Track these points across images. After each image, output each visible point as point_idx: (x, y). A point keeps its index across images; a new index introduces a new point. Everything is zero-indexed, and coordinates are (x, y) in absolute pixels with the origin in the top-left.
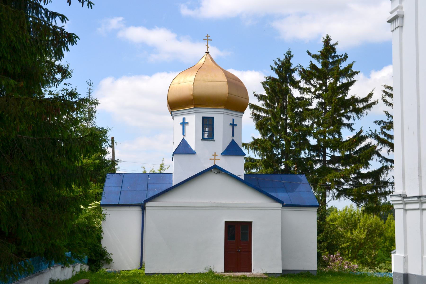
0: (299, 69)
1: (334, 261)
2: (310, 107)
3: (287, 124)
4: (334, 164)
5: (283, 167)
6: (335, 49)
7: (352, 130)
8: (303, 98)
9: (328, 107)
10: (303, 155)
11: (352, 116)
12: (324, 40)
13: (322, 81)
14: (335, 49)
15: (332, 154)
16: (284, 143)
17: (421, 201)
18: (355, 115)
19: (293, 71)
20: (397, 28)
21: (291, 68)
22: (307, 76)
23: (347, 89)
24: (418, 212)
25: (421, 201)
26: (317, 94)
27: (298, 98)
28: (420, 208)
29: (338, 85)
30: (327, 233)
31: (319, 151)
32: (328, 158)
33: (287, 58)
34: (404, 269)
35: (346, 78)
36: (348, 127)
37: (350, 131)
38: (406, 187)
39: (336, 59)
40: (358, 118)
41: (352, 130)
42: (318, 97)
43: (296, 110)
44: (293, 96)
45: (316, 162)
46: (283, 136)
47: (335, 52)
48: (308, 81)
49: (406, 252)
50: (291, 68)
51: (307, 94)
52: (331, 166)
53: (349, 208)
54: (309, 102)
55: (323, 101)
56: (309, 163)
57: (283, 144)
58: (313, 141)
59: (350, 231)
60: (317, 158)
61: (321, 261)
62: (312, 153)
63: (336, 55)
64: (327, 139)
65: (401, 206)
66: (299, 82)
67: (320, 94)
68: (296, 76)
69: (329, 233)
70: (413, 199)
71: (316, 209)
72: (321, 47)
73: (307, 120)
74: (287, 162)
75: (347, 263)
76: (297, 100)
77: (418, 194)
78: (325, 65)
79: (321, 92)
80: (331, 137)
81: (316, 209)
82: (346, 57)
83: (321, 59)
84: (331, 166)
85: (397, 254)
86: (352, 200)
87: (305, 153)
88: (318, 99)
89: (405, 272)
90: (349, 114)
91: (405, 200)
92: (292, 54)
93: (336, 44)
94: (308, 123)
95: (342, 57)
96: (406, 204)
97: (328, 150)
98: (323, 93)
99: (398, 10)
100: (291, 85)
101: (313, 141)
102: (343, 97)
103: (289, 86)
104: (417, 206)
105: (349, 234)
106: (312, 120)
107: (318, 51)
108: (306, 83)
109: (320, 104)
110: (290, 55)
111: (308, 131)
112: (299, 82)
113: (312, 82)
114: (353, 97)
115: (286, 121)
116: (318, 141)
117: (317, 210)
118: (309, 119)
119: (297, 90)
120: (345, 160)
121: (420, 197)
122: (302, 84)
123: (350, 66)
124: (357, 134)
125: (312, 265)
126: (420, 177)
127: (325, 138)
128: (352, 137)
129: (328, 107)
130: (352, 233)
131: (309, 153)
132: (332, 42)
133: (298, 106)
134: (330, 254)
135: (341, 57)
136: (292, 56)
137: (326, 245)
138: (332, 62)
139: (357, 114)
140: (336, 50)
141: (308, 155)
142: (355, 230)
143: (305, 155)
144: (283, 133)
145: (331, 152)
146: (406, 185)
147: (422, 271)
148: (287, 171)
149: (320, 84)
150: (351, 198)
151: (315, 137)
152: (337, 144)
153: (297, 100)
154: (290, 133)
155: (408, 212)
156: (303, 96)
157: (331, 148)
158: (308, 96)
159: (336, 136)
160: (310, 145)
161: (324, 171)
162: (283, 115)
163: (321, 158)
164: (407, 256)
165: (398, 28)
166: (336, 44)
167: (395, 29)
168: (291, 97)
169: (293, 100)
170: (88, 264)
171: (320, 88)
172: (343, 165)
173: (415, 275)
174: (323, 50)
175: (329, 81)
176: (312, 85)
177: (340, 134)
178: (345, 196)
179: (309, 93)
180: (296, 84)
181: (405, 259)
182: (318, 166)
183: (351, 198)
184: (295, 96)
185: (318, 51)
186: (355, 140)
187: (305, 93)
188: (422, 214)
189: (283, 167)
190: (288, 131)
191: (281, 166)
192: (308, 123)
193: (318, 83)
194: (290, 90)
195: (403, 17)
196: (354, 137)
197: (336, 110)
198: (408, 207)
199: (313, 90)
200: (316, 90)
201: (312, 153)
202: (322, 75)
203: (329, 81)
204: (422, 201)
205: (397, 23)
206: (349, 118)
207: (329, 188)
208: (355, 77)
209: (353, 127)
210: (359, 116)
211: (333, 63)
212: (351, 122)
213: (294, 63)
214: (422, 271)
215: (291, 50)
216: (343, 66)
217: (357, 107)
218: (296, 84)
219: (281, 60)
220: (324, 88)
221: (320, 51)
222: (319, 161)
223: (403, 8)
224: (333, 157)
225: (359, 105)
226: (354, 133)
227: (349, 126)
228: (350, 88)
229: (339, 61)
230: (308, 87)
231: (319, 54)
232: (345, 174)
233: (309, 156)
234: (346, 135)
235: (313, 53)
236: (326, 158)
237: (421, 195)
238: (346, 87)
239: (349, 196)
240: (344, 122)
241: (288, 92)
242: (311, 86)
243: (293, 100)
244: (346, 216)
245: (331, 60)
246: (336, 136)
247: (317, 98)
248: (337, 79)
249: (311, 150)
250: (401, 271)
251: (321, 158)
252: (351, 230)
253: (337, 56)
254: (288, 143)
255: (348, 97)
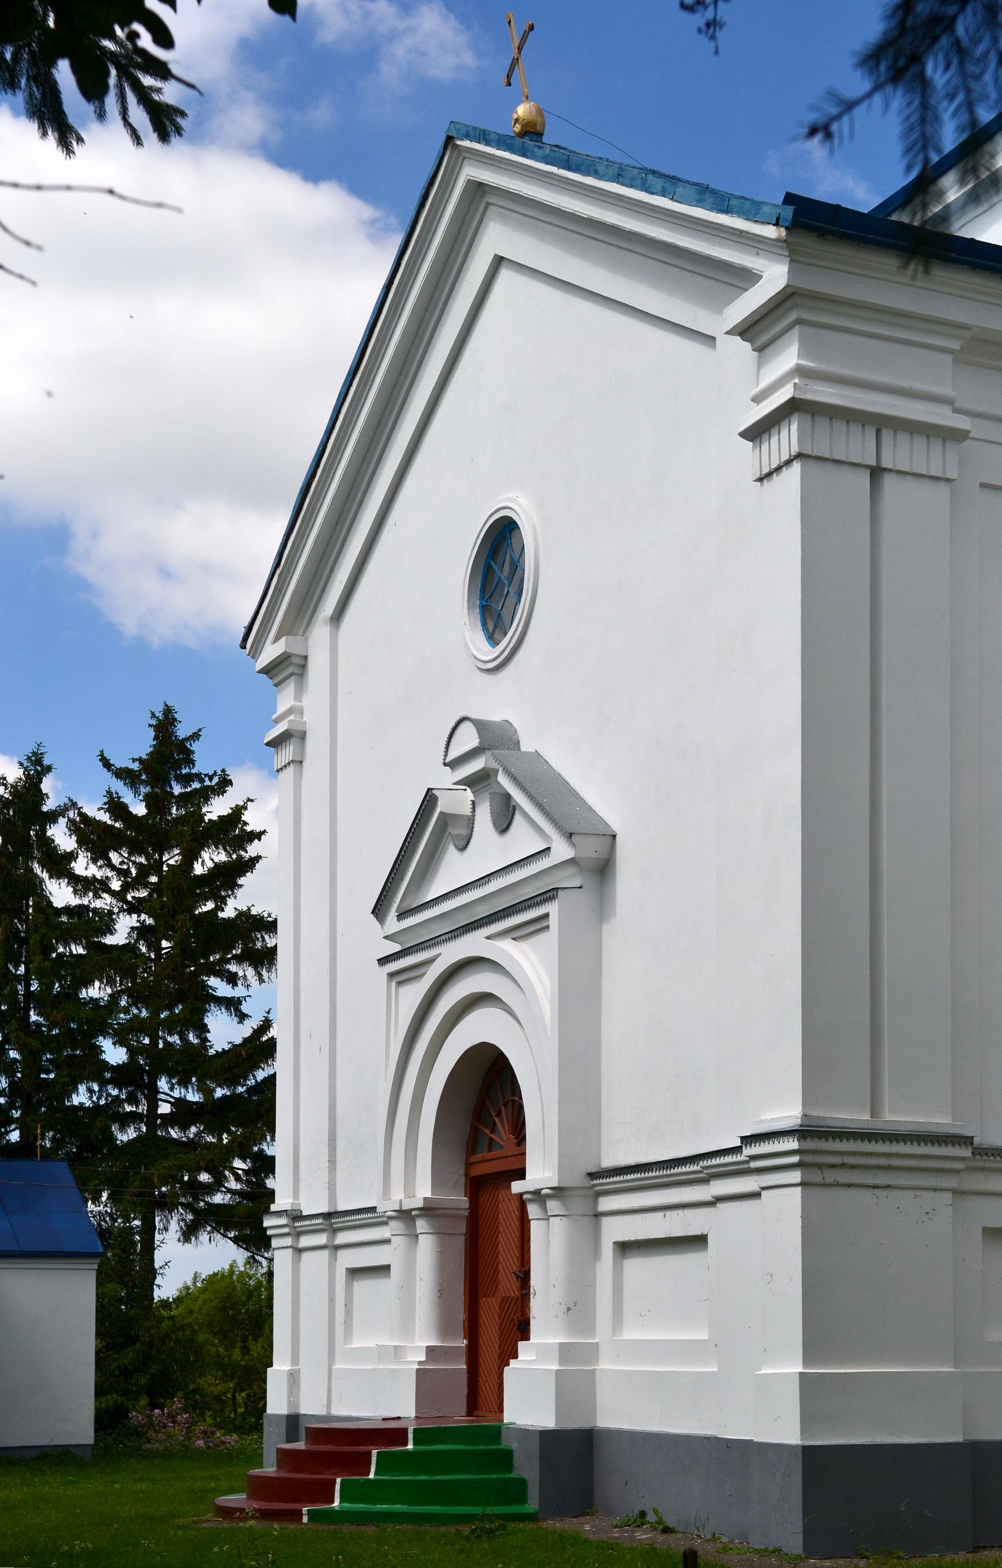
0: (71, 815)
1: (165, 1426)
2: (109, 940)
3: (28, 994)
4: (184, 1128)
5: (15, 1136)
6: (193, 752)
7: (242, 1017)
8: (87, 908)
9: (165, 944)
10: (81, 1097)
11: (241, 973)
12: (154, 722)
13: (147, 859)
14: (193, 752)
15: (176, 1094)
16: (17, 1057)
17: (331, 1225)
18: (250, 972)
19: (52, 817)
20: (289, 764)
21: (45, 809)
22: (95, 838)
23: (233, 886)
24: (325, 1253)
25: (331, 1225)
26: (129, 898)
27: (68, 910)
28: (330, 1243)
29: (198, 869)
30: (151, 1345)
31: (139, 1086)
32: (165, 1108)
33: (28, 776)
34: (290, 1403)
35: (225, 850)
36: (227, 1009)
37: (236, 1020)
38: (301, 1190)
39: (196, 785)
40: (261, 981)
41: (242, 1017)
42: (133, 908)
43: (61, 950)
44: (50, 903)
45: (126, 1120)
46: (12, 1036)
47: (190, 762)
48: (99, 855)
49: (295, 1359)
50: (45, 809)
51: (96, 896)
52: (174, 1133)
53: (242, 1269)
54: (106, 922)
55: (150, 921)
56: (98, 1124)
57: (15, 1060)
58: (114, 1054)
59: (239, 1344)
60: (128, 1108)
61: (108, 1420)
62: (115, 1092)
63: (193, 771)
64: (161, 1046)
65: (288, 1241)
66: (71, 856)
67: (139, 900)
68: (62, 837)
69: (157, 1344)
70: (314, 1222)
71: (94, 1265)
72: (144, 744)
73: (97, 984)
74: (28, 1119)
75: (205, 1432)
76: (64, 919)
77: (324, 1209)
78: (156, 803)
79: (143, 894)
80: (175, 1039)
81: (94, 1265)
82: (225, 783)
83: (143, 782)
84: (174, 1133)
85: (275, 1367)
86: (236, 1240)
87: (90, 1091)
88: (135, 916)
89: (292, 1412)
90: (233, 968)
91: (297, 1224)
92: (46, 762)
93: (196, 736)
94: (96, 991)
95: (214, 783)
96: (299, 1234)
97: (163, 1084)
98: (150, 895)
99: (292, 717)
100: (43, 866)
101: (114, 1054)
102: (213, 912)
103: (37, 868)
104: (321, 1239)
105: (237, 1353)
106: (111, 982)
107: (134, 760)
108: (94, 861)
109: (142, 931)
110: (41, 764)
111: (99, 1019)
112: (71, 856)
113: (115, 857)
114: (241, 914)
115: (28, 985)
116: (132, 1052)
117: (96, 1267)
118: (101, 982)
119: (64, 882)
120: (213, 1114)
121: (328, 1216)
122: (83, 866)
123: (238, 811)
124: (255, 1031)
125: (79, 1427)
126: (332, 1163)
127: (154, 1042)
128: (238, 1041)
129: (165, 944)
130: (246, 1351)
131: (100, 1090)
132: (182, 731)
133: (68, 936)
134: (153, 1406)
135: (211, 779)
136: (49, 769)
137: (143, 1381)
138: (181, 794)
139: (256, 968)
140: (196, 757)
141: (99, 1098)
142: (256, 1339)
143: (91, 1098)
144: (14, 1025)
145: (172, 1089)
146: (302, 1184)
147: (329, 1405)
148: (26, 1149)
149: (139, 866)
150: (232, 1235)
151: (120, 1040)
152: (193, 1063)
153: (64, 919)
154: (38, 1025)
155: (306, 1256)
156: (85, 902)
157: (171, 1076)
158: (105, 902)
159: (192, 1038)
160: (105, 1065)
161: (150, 1145)
162: (17, 967)
163: (143, 1108)
164: (299, 1370)
165: (292, 766)
166: (196, 736)
167: (285, 766)
168: (45, 904)
169: (47, 919)
170: (787, 228)
171: (140, 881)
172: (210, 1130)
173: (313, 1416)
174: (150, 754)
175: (172, 858)
176: (113, 868)
177: (202, 1029)
178: (215, 1229)
179: (105, 895)
180: (59, 865)
181: (293, 1378)
182: (127, 1135)
183: (232, 1235)
184: (58, 903)
185: (134, 760)
186: (244, 1053)
187: (91, 894)
188: (333, 1259)
189: (15, 1136)
190: (34, 1017)
191: (8, 1133)
192: (96, 991)
193: (134, 863)
194: (42, 881)
195: (303, 736)
196: (246, 1040)
197: (184, 952)
198: (305, 1241)
199: (116, 885)
200: (126, 888)
201: (115, 1092)
202: (143, 836)
203: (172, 858)
204: (335, 1226)
205: (287, 753)
206: (232, 979)
207: (167, 1205)
208: (253, 849)
209: (244, 1008)
210: (264, 973)
211: (183, 799)
212: (239, 991)
213: (53, 791)
214: (329, 1405)
215: (43, 750)
216: (216, 809)
217: (259, 945)
218: (59, 865)
219: (11, 780)
220: (154, 879)
221: (140, 760)
222: (135, 1118)
223: (305, 712)
224: (179, 1103)
225: (266, 937)
226: (246, 1030)
227: (233, 1005)
228: (241, 881)
229: (205, 795)
230: (99, 875)
231: (136, 766)
232: (212, 1160)
233: (102, 1102)
234: (223, 1032)
235: (121, 761)
236: (157, 1107)
237: (332, 1210)
238: (227, 877)
239: (227, 1229)
240: (219, 993)
241: (36, 887)
242: (110, 873)
243: (47, 919)
244: (229, 1296)
245: (177, 790)
246: (192, 1038)
247: (130, 912)
248: (191, 856)
249: (109, 1082)
250: (284, 1411)
251: (143, 1108)
252: (244, 1339)
253: (199, 777)
254: (31, 1056)
255: (228, 912)
